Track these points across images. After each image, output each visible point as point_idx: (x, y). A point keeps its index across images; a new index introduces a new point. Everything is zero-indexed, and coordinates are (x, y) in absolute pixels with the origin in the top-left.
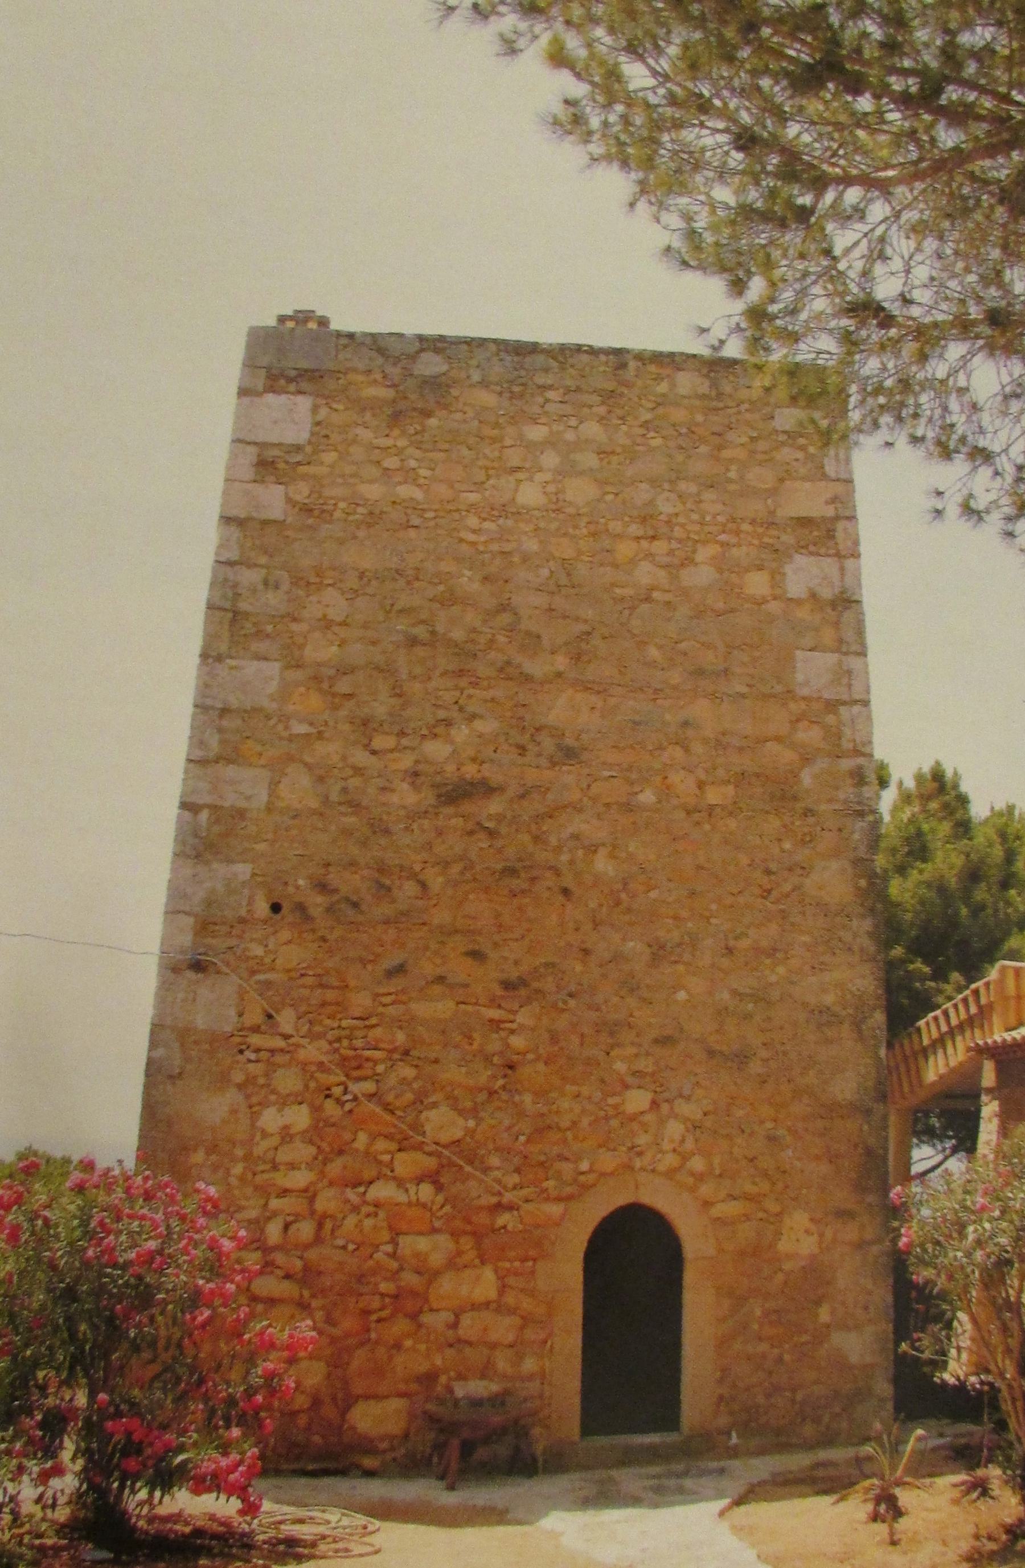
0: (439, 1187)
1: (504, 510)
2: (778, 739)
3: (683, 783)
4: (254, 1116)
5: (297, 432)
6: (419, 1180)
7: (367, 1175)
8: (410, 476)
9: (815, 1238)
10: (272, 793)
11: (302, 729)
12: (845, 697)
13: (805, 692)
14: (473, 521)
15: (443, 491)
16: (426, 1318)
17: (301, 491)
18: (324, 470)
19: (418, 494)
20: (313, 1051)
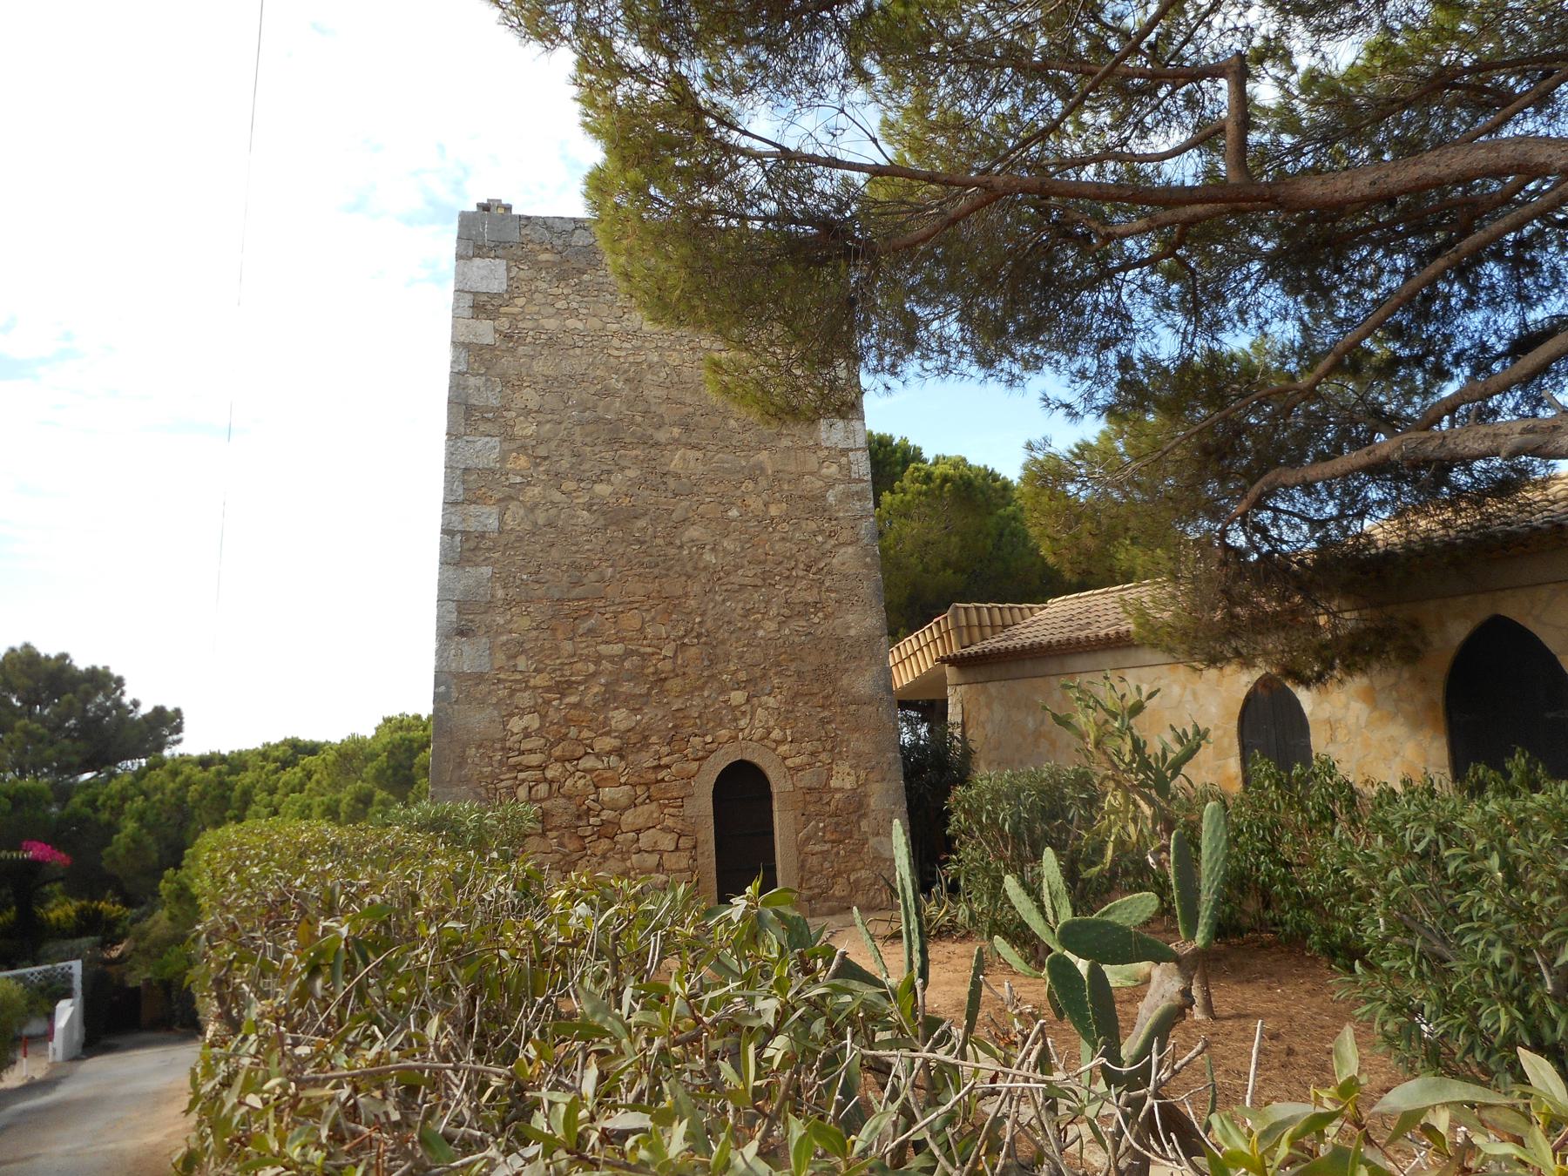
0: (622, 757)
2: (812, 474)
3: (755, 504)
4: (505, 724)
5: (498, 285)
6: (609, 754)
7: (577, 755)
8: (574, 313)
9: (853, 778)
10: (501, 521)
11: (518, 479)
12: (852, 446)
14: (616, 343)
16: (619, 838)
17: (504, 324)
19: (580, 325)
20: (539, 680)
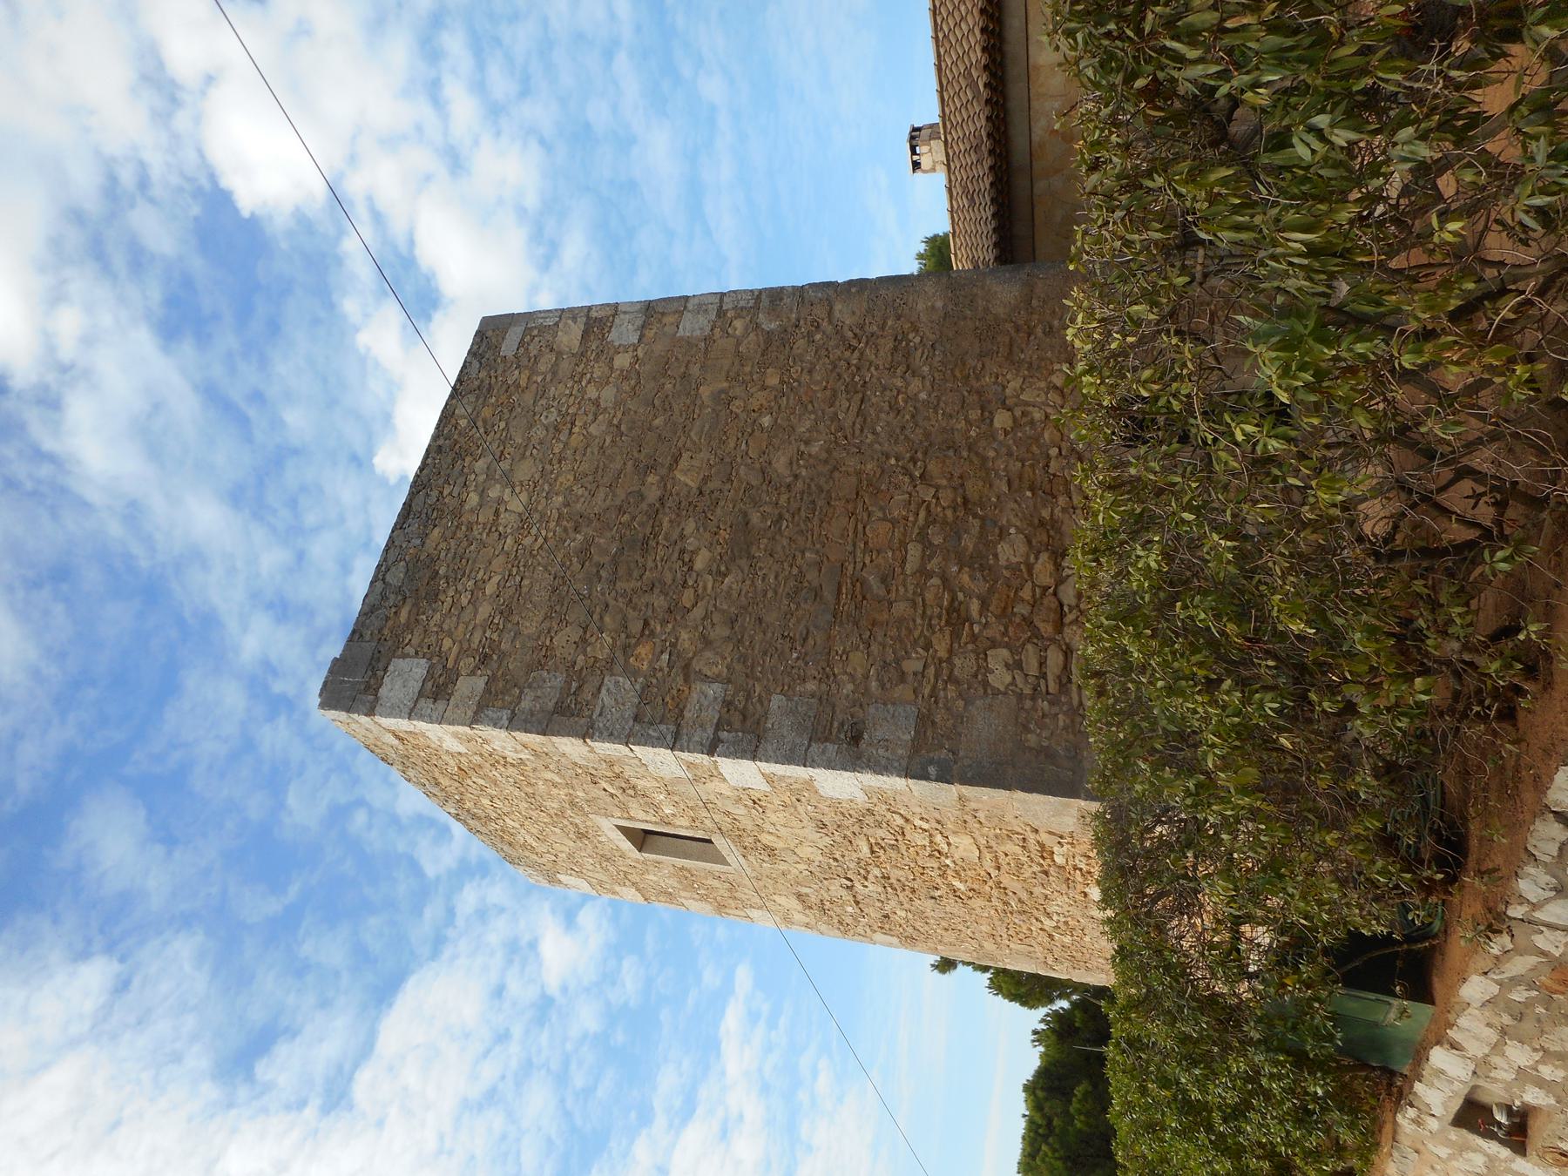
1: (524, 523)
2: (738, 344)
3: (760, 398)
7: (1054, 605)
8: (480, 586)
13: (708, 329)
14: (527, 541)
15: (498, 563)
17: (467, 663)
18: (455, 649)
